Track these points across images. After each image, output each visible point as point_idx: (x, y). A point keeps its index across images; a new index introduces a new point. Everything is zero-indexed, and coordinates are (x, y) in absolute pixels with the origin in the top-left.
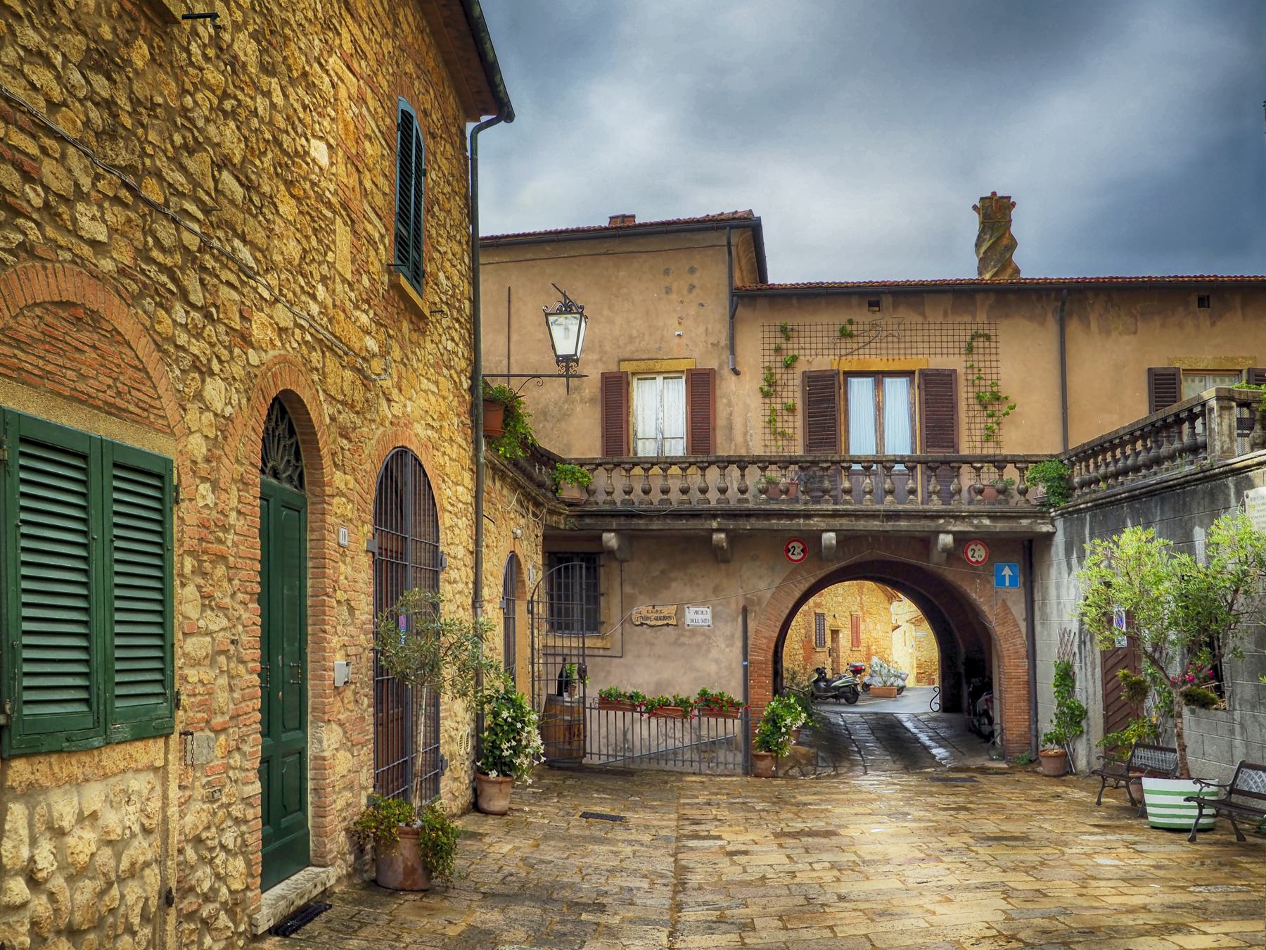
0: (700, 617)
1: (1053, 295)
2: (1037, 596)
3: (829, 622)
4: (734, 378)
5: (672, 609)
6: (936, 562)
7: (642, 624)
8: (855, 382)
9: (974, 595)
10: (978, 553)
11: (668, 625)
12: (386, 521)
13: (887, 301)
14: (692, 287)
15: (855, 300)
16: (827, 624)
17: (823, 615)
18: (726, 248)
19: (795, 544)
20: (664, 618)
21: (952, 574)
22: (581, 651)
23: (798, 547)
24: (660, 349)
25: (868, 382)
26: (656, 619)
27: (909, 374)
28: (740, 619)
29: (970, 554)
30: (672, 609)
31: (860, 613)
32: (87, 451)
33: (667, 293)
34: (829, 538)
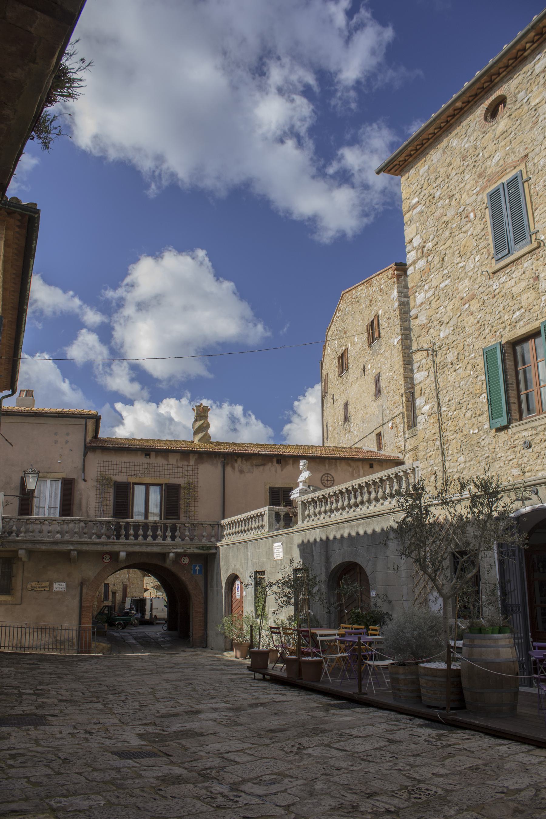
0: (61, 587)
1: (221, 456)
2: (209, 578)
3: (111, 587)
4: (83, 482)
5: (48, 583)
6: (168, 564)
7: (32, 590)
8: (136, 487)
9: (183, 578)
10: (186, 560)
11: (45, 590)
12: (495, 376)
13: (153, 454)
14: (67, 442)
15: (139, 453)
16: (110, 589)
17: (108, 584)
18: (84, 426)
19: (107, 556)
20: (43, 587)
21: (174, 569)
22: (35, 630)
23: (108, 557)
24: (50, 468)
25: (143, 487)
26: (40, 588)
27: (160, 485)
28: (79, 588)
29: (182, 560)
30: (48, 583)
31: (128, 583)
32: (374, 434)
33: (55, 443)
34: (123, 555)
